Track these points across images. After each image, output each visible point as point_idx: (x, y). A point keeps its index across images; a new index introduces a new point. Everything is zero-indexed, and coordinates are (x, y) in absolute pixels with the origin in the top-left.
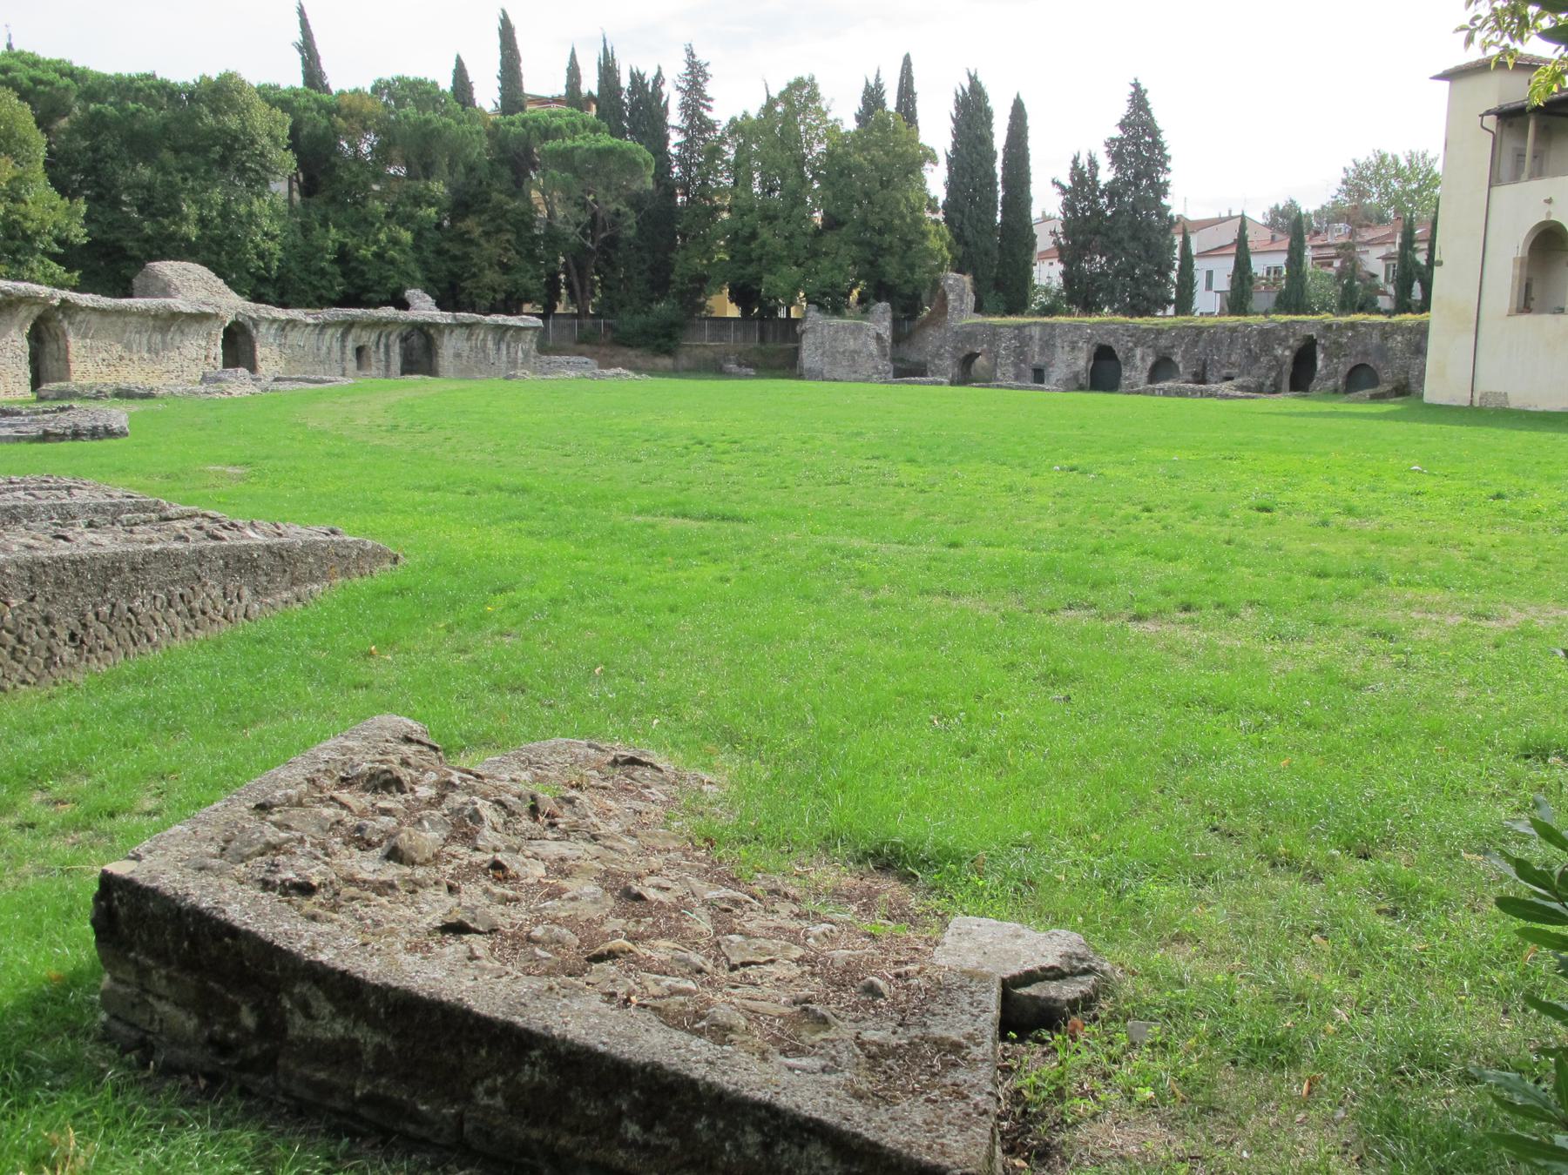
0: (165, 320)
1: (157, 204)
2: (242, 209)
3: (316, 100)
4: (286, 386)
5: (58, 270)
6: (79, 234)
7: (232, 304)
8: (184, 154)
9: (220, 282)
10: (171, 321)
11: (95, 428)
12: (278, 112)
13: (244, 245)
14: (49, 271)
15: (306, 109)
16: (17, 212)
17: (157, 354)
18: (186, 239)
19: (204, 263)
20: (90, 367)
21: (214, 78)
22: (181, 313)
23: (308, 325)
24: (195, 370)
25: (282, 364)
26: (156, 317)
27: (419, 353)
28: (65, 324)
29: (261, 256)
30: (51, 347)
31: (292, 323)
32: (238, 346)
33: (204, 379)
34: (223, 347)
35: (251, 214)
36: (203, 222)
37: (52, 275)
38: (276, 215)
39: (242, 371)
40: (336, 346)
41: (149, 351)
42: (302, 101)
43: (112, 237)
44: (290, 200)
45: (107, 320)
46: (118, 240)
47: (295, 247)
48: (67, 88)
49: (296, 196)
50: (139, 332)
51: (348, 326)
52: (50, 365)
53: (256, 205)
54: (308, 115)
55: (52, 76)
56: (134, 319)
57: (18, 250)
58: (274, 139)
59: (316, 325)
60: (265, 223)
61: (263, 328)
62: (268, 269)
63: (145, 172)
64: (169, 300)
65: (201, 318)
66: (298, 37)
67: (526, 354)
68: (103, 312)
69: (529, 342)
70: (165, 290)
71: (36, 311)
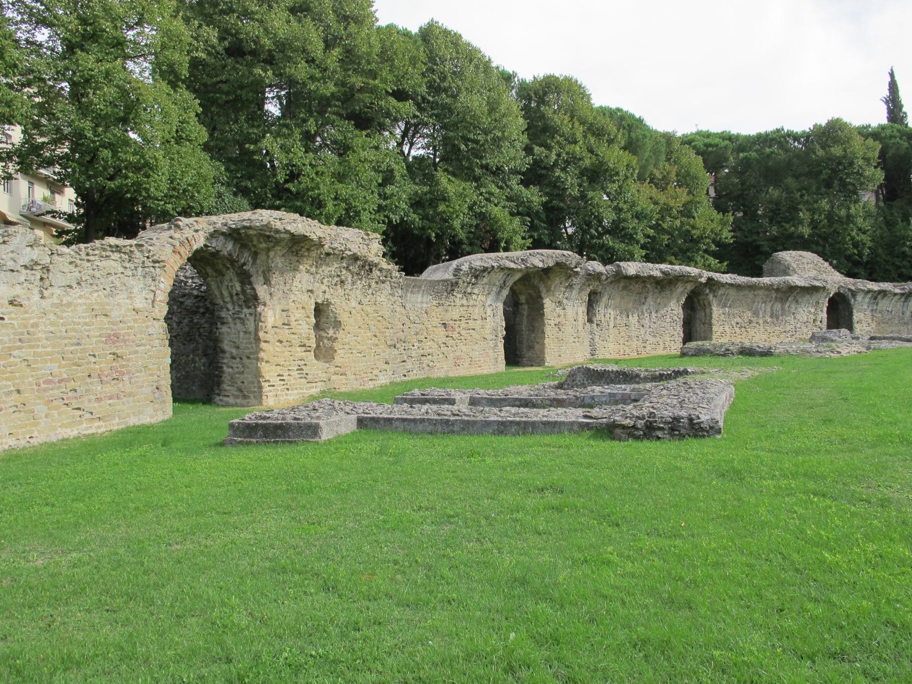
0: (785, 292)
1: (783, 214)
2: (843, 212)
3: (899, 131)
4: (884, 344)
5: (713, 261)
6: (727, 236)
7: (835, 280)
8: (803, 178)
9: (826, 264)
10: (790, 293)
11: (677, 419)
12: (870, 141)
13: (844, 238)
14: (707, 263)
15: (891, 137)
16: (689, 224)
17: (777, 319)
18: (801, 237)
19: (813, 252)
20: (727, 328)
21: (823, 124)
22: (797, 286)
23: (895, 294)
24: (805, 330)
25: (874, 325)
26: (778, 290)
28: (711, 297)
29: (856, 245)
30: (700, 314)
31: (883, 293)
32: (839, 312)
33: (813, 338)
34: (828, 313)
35: (849, 216)
36: (814, 224)
37: (709, 266)
38: (868, 215)
39: (844, 331)
41: (771, 316)
42: (888, 132)
43: (750, 240)
44: (877, 205)
45: (742, 293)
46: (755, 241)
47: (882, 238)
48: (726, 147)
49: (881, 204)
50: (765, 302)
52: (699, 328)
53: (852, 211)
54: (893, 141)
55: (717, 140)
56: (761, 292)
57: (688, 250)
58: (867, 160)
59: (902, 294)
60: (860, 221)
61: (859, 298)
62: (860, 255)
63: (774, 193)
64: (787, 278)
65: (812, 290)
66: (886, 93)
68: (738, 287)
70: (786, 271)
71: (690, 287)
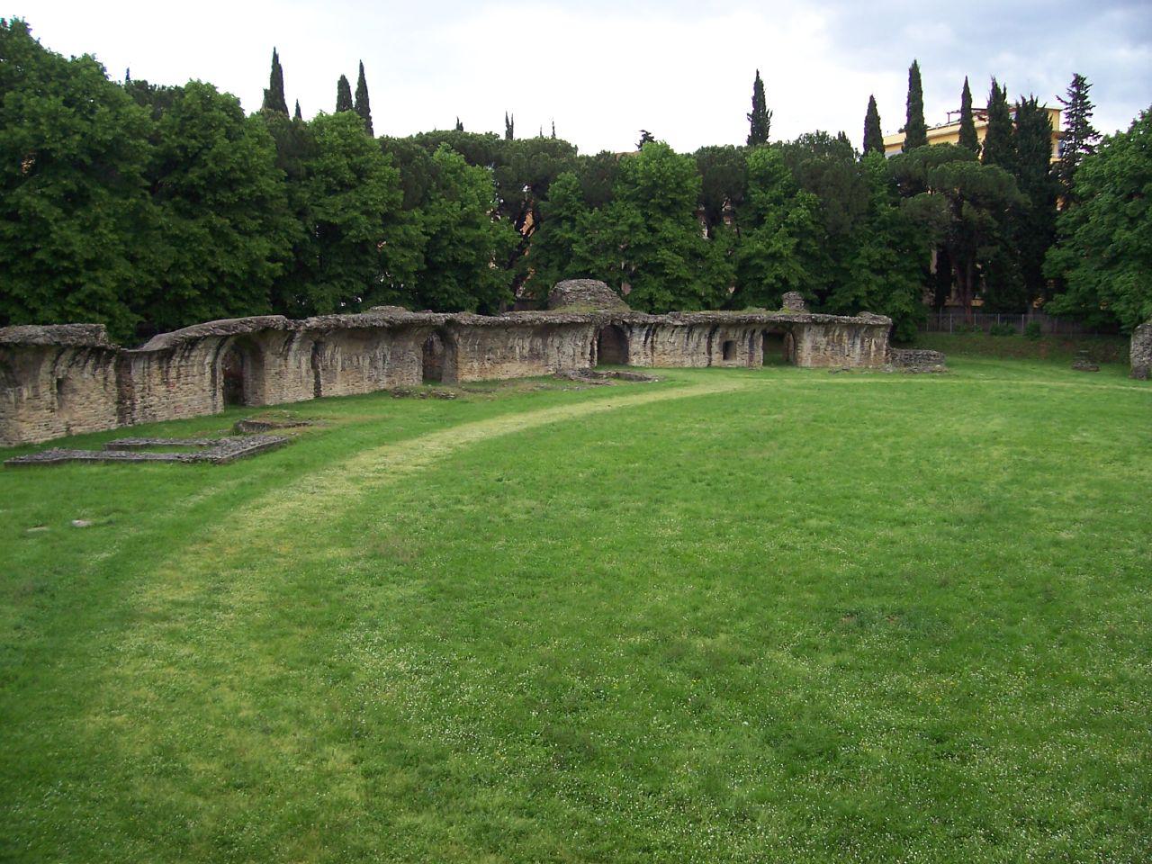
7: (613, 308)
27: (779, 345)
31: (662, 326)
40: (704, 342)
51: (714, 327)
59: (683, 326)
61: (636, 331)
67: (879, 348)
69: (882, 339)
